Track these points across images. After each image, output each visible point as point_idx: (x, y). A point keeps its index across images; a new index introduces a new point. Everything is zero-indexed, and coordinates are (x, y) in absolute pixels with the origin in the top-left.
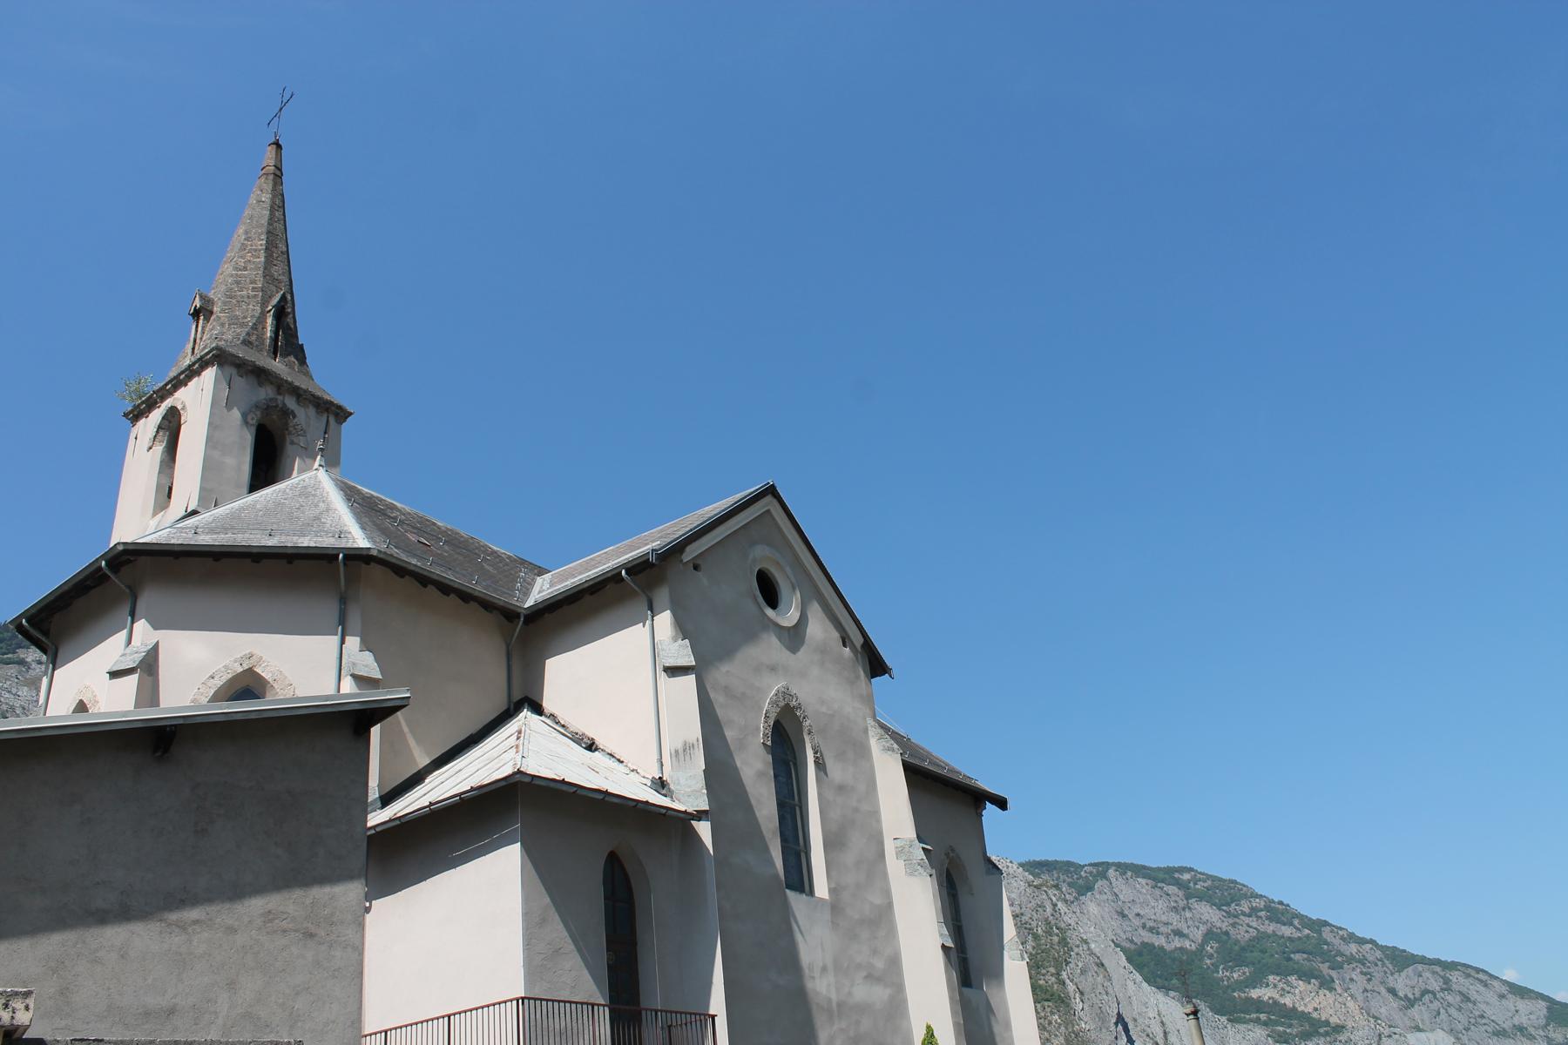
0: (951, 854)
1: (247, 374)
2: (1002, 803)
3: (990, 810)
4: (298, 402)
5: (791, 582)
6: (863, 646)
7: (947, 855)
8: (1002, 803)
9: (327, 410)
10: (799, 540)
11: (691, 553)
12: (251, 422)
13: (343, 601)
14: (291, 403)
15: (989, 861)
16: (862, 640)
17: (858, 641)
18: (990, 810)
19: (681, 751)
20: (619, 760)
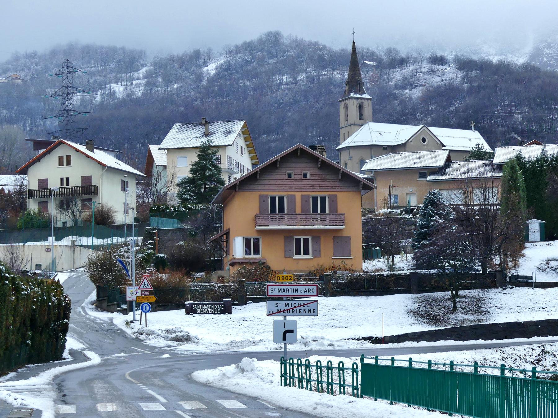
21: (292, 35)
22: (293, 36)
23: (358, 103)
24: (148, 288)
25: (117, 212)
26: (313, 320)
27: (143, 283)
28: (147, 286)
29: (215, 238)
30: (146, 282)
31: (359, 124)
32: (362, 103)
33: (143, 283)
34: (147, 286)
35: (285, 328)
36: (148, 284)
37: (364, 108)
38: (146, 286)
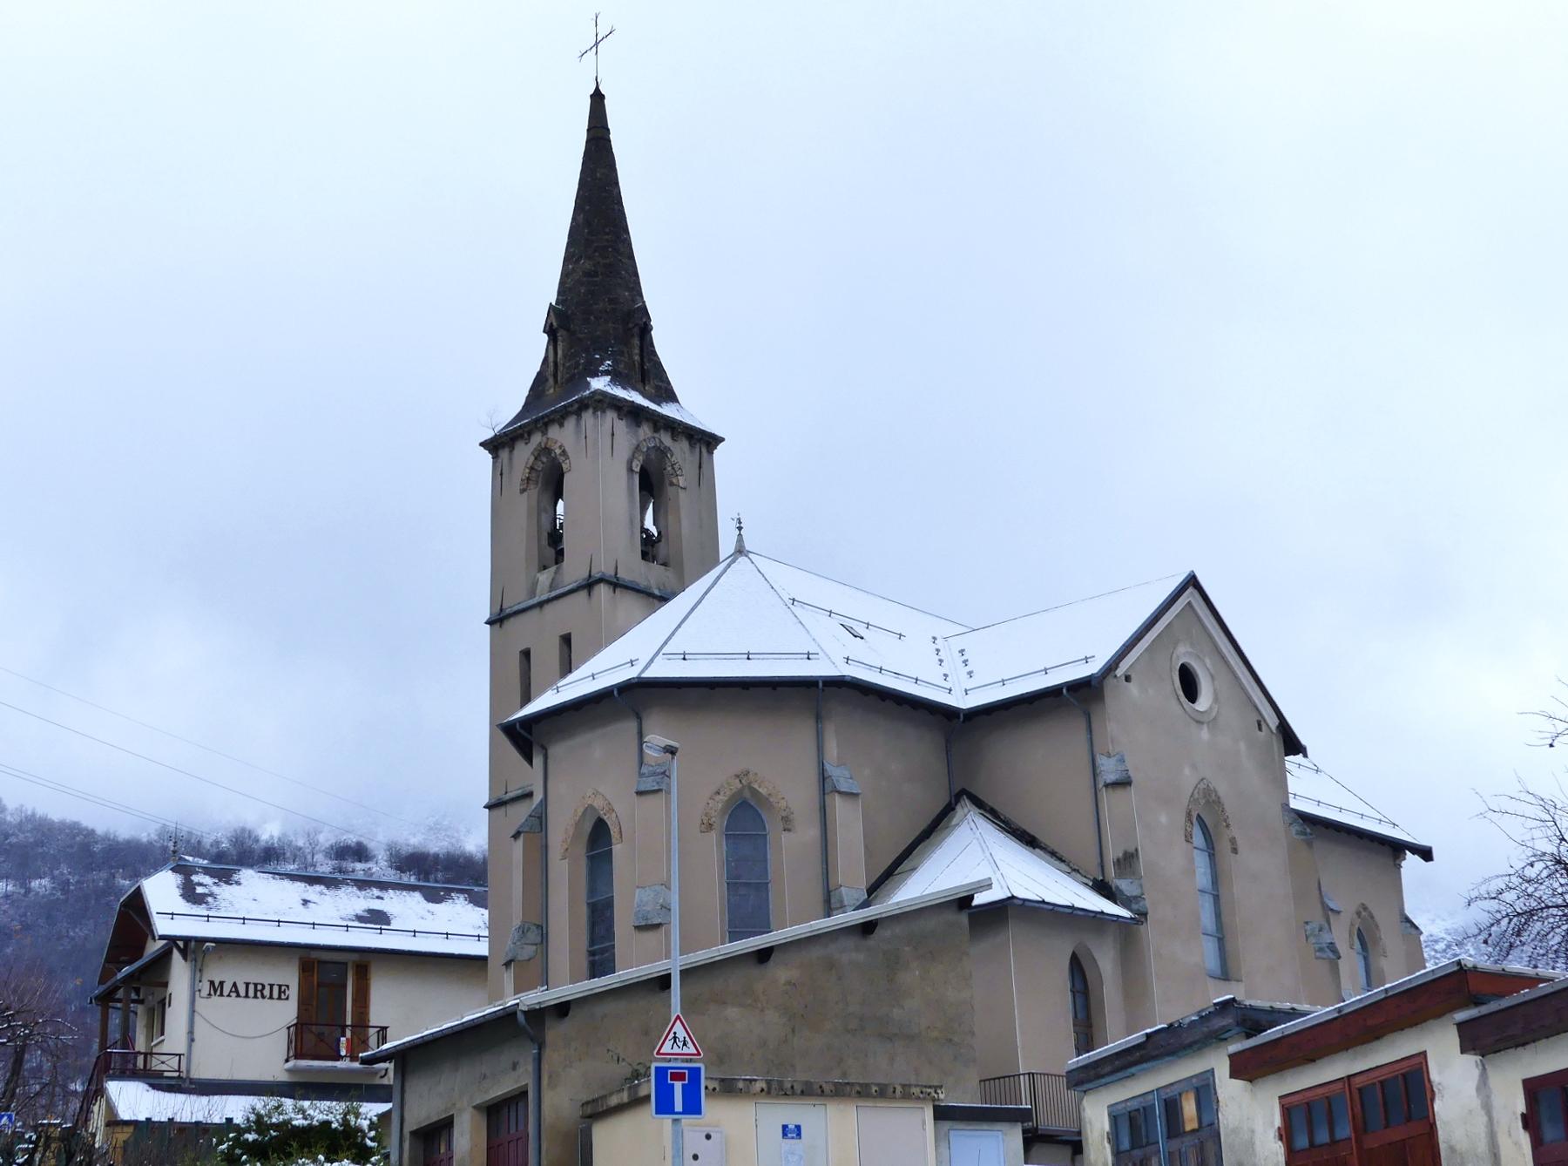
0: (1364, 913)
1: (625, 416)
2: (1426, 854)
3: (1411, 862)
4: (674, 438)
5: (1208, 669)
6: (1278, 727)
7: (1359, 914)
8: (1426, 854)
9: (700, 440)
10: (1217, 627)
11: (1120, 671)
12: (636, 470)
13: (818, 718)
14: (666, 439)
15: (1408, 920)
16: (1277, 722)
17: (1273, 722)
18: (1411, 862)
19: (1122, 861)
20: (740, 528)
21: (24, 808)
22: (27, 810)
23: (637, 448)
24: (686, 1050)
25: (615, 592)
26: (616, 1058)
27: (671, 1035)
28: (685, 1044)
29: (1420, 982)
30: (681, 1034)
31: (643, 583)
32: (662, 452)
33: (671, 1035)
34: (685, 1044)
35: (158, 913)
36: (687, 1039)
37: (671, 490)
38: (681, 1044)
